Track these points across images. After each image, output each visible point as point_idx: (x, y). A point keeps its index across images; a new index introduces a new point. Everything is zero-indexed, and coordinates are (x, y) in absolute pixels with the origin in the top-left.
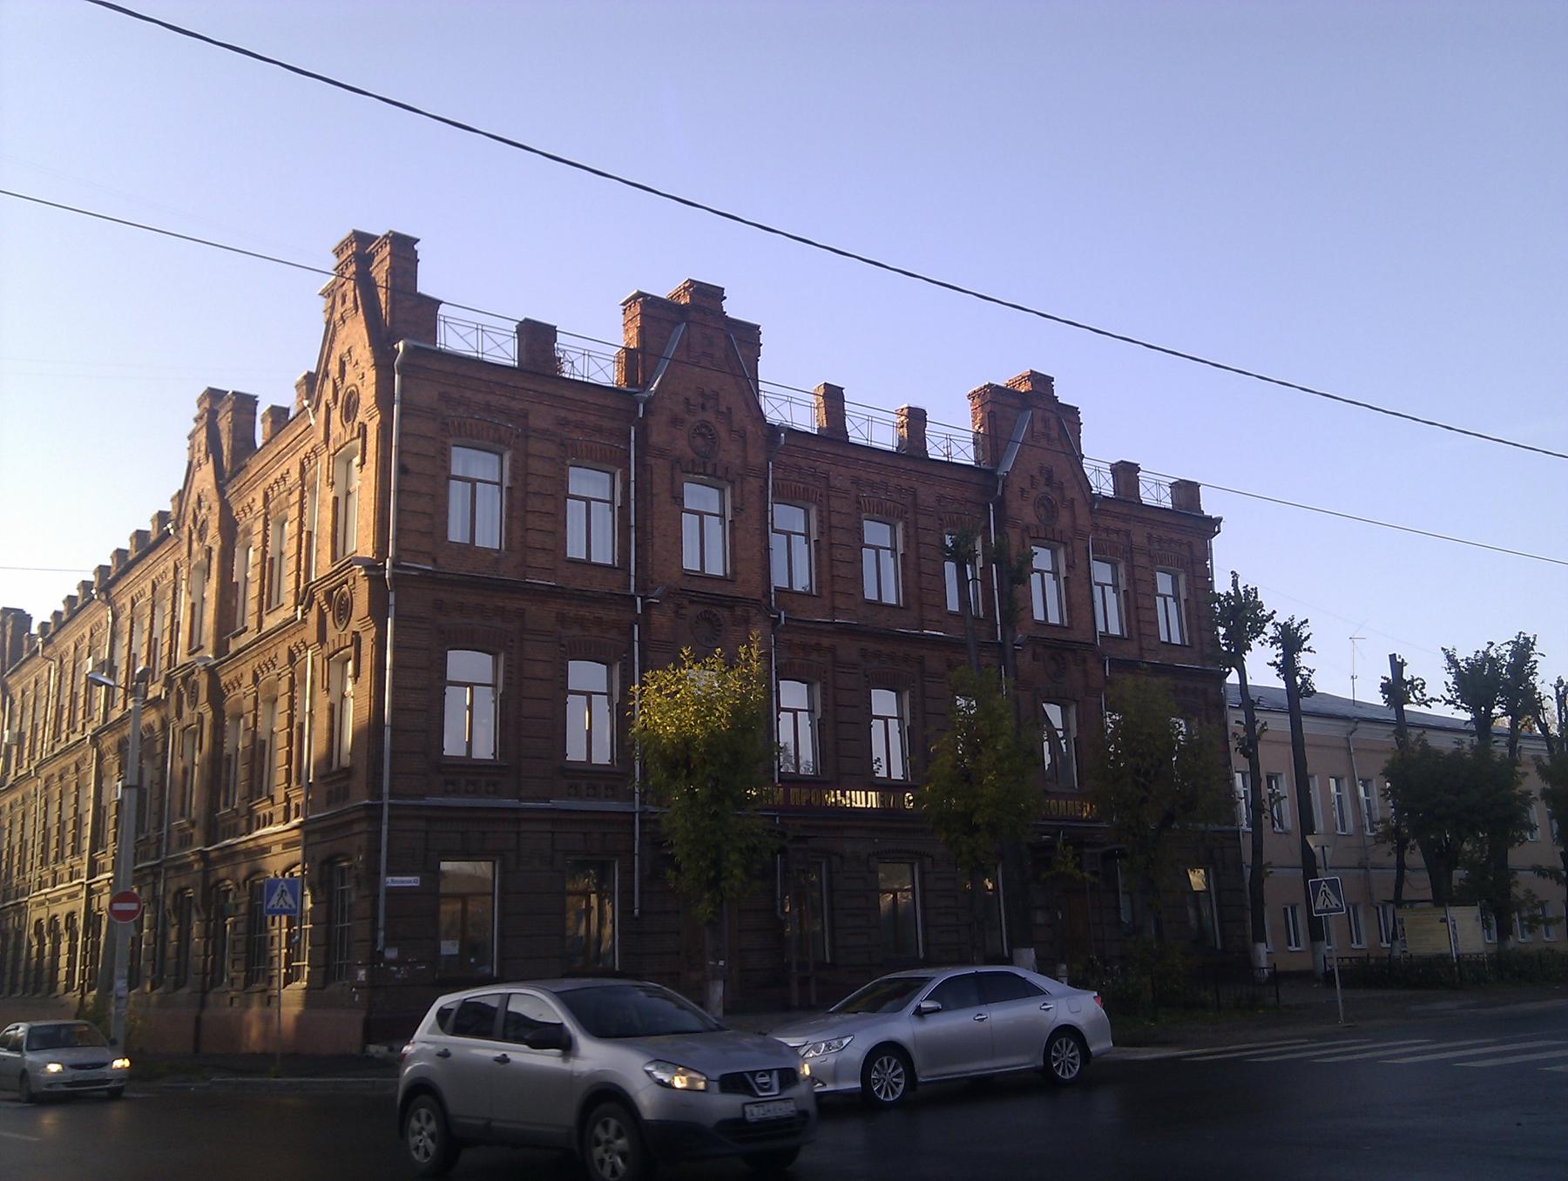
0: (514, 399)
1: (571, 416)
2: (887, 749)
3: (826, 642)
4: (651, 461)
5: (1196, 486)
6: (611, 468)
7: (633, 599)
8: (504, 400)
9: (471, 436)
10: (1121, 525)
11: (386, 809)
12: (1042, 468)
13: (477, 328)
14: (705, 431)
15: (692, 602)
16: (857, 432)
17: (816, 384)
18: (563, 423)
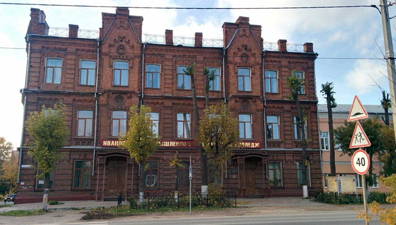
0: (63, 45)
1: (80, 48)
2: (182, 131)
3: (160, 101)
4: (103, 57)
5: (312, 44)
6: (219, 67)
7: (224, 99)
8: (61, 46)
9: (51, 56)
10: (277, 59)
11: (97, 148)
12: (243, 45)
13: (58, 28)
14: (244, 56)
15: (113, 93)
16: (290, 48)
17: (276, 41)
18: (77, 50)
